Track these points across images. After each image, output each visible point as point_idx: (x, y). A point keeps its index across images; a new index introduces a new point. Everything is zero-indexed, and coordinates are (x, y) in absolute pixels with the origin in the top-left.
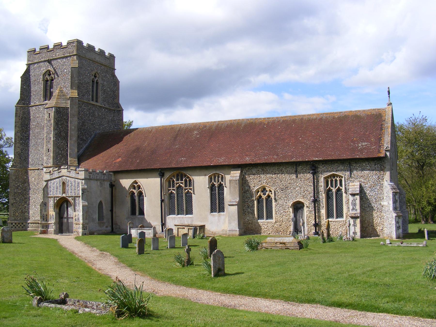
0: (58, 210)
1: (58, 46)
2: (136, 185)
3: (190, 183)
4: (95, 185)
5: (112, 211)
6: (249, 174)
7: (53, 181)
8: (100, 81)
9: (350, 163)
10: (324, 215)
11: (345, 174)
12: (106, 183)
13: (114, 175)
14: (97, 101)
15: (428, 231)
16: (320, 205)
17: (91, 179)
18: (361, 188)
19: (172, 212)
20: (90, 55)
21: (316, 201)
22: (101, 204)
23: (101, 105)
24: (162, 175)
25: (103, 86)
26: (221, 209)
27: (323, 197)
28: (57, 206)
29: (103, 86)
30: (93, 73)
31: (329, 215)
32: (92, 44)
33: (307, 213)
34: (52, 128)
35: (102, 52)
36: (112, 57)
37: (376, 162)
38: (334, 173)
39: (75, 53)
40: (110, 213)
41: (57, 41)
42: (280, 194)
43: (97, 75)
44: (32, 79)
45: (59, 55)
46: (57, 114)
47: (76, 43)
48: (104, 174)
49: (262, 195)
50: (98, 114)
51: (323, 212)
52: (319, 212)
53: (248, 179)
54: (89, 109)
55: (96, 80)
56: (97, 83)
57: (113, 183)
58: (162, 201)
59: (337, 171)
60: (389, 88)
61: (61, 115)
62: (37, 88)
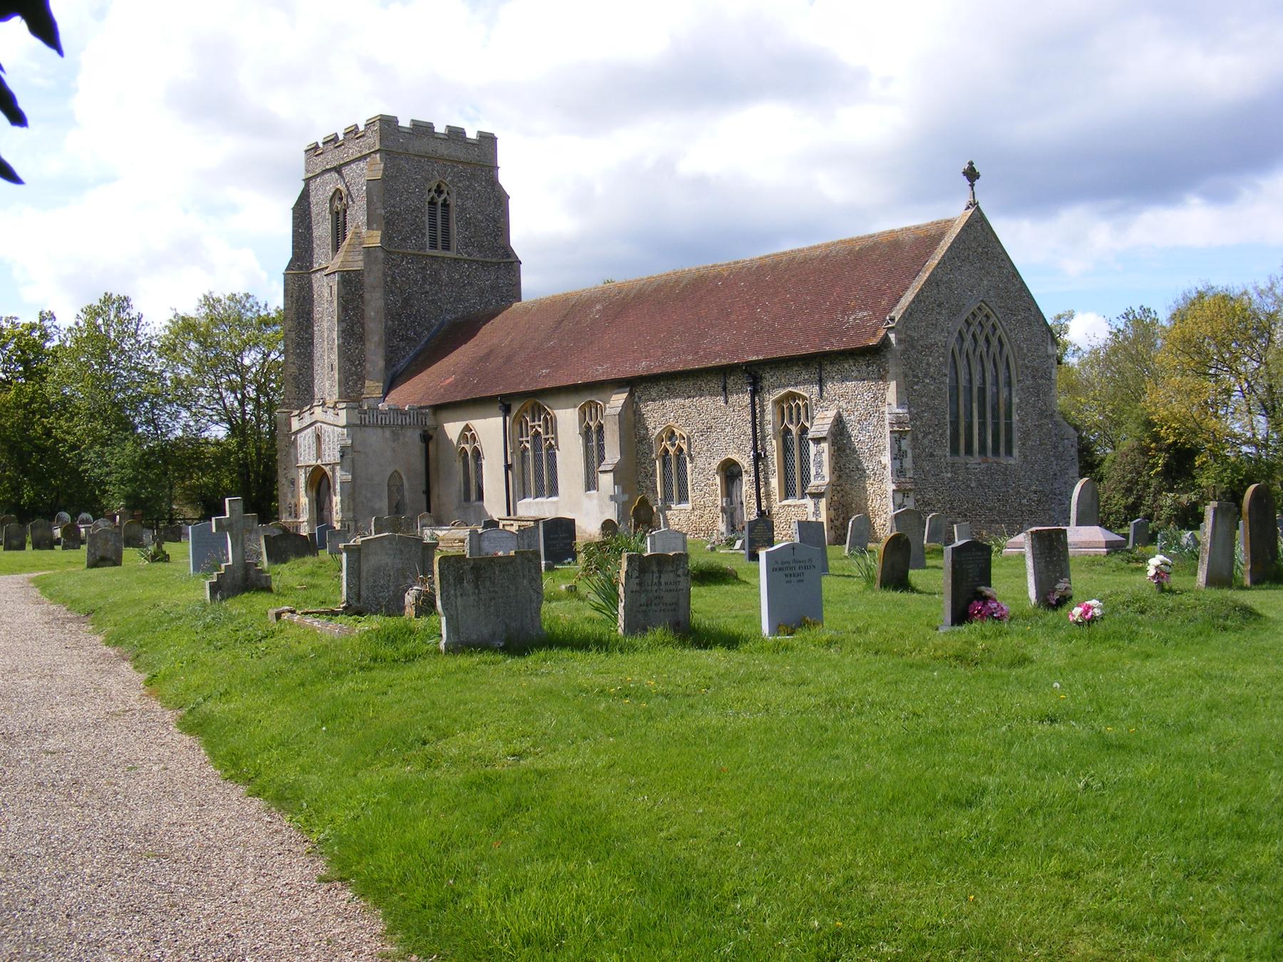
1: (353, 132)
2: (469, 434)
3: (551, 425)
4: (376, 439)
6: (647, 400)
7: (303, 434)
8: (452, 201)
9: (820, 365)
10: (777, 491)
11: (808, 391)
12: (409, 433)
13: (435, 413)
14: (447, 247)
16: (766, 466)
17: (365, 426)
18: (839, 423)
20: (418, 146)
21: (758, 458)
23: (459, 256)
24: (507, 411)
25: (463, 209)
27: (773, 447)
29: (463, 209)
31: (788, 492)
33: (746, 486)
35: (456, 134)
36: (488, 141)
37: (867, 358)
38: (790, 389)
39: (377, 147)
40: (424, 497)
41: (349, 123)
42: (698, 444)
43: (443, 187)
46: (345, 287)
47: (378, 123)
48: (404, 413)
49: (669, 448)
50: (451, 278)
51: (774, 482)
52: (767, 483)
53: (643, 411)
54: (423, 268)
56: (445, 205)
57: (430, 432)
58: (508, 467)
59: (796, 385)
60: (971, 174)
61: (350, 284)
62: (322, 230)
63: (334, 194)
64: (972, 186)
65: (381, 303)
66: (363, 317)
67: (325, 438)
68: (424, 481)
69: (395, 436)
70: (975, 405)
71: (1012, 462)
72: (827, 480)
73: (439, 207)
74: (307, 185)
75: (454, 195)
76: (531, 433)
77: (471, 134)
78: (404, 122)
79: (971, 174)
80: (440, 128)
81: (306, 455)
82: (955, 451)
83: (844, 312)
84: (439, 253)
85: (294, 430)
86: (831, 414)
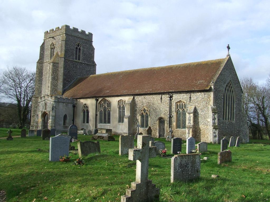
0: (43, 119)
8: (81, 48)
12: (69, 104)
14: (79, 60)
18: (195, 109)
19: (101, 122)
20: (74, 34)
22: (65, 117)
26: (123, 122)
27: (174, 114)
28: (43, 117)
29: (83, 51)
30: (77, 44)
34: (51, 74)
35: (83, 32)
36: (90, 35)
40: (72, 121)
41: (51, 28)
43: (79, 45)
44: (46, 47)
45: (57, 34)
46: (53, 67)
50: (80, 67)
55: (79, 47)
56: (80, 49)
60: (229, 48)
62: (47, 53)
63: (52, 44)
64: (229, 51)
65: (63, 72)
66: (58, 75)
67: (48, 104)
68: (73, 117)
69: (67, 105)
70: (227, 107)
71: (234, 122)
72: (192, 124)
73: (78, 49)
74: (44, 41)
75: (82, 47)
76: (103, 107)
77: (87, 33)
78: (71, 27)
79: (229, 48)
80: (80, 30)
81: (41, 109)
82: (223, 119)
83: (196, 80)
84: (77, 61)
85: (39, 102)
86: (193, 107)
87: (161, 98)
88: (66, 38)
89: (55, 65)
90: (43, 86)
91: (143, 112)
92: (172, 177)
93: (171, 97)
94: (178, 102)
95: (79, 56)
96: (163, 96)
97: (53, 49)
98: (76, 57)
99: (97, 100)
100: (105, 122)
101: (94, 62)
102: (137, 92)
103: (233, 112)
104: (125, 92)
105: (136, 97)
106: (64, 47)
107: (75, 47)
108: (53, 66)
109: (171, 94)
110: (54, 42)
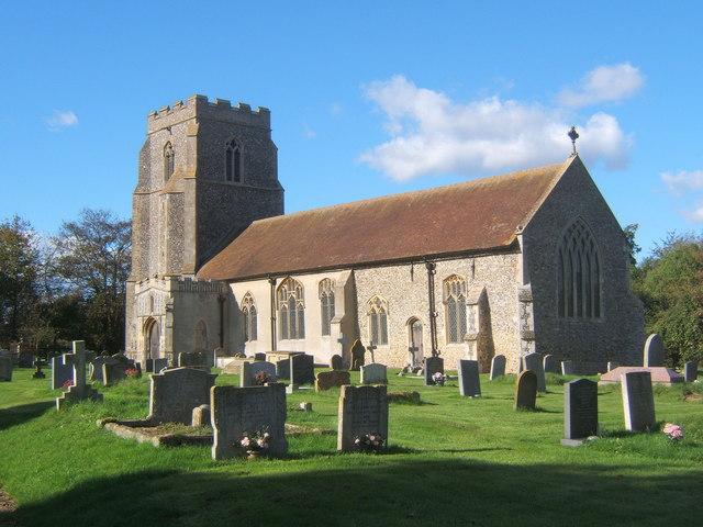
5: (221, 335)
8: (242, 151)
14: (237, 180)
15: (313, 384)
18: (484, 295)
19: (284, 336)
21: (433, 317)
27: (441, 309)
30: (229, 140)
32: (224, 97)
35: (245, 109)
36: (265, 113)
56: (237, 153)
72: (478, 331)
73: (232, 155)
76: (288, 298)
78: (213, 100)
82: (562, 313)
84: (233, 183)
87: (412, 272)
88: (199, 130)
89: (176, 198)
90: (151, 252)
91: (375, 306)
92: (340, 439)
93: (431, 268)
94: (447, 279)
95: (237, 171)
96: (416, 267)
97: (169, 159)
98: (229, 174)
99: (274, 283)
100: (293, 337)
101: (276, 184)
102: (359, 258)
103: (597, 297)
104: (333, 260)
105: (357, 273)
106: (195, 152)
107: (226, 148)
108: (172, 200)
109: (430, 261)
110: (172, 139)
